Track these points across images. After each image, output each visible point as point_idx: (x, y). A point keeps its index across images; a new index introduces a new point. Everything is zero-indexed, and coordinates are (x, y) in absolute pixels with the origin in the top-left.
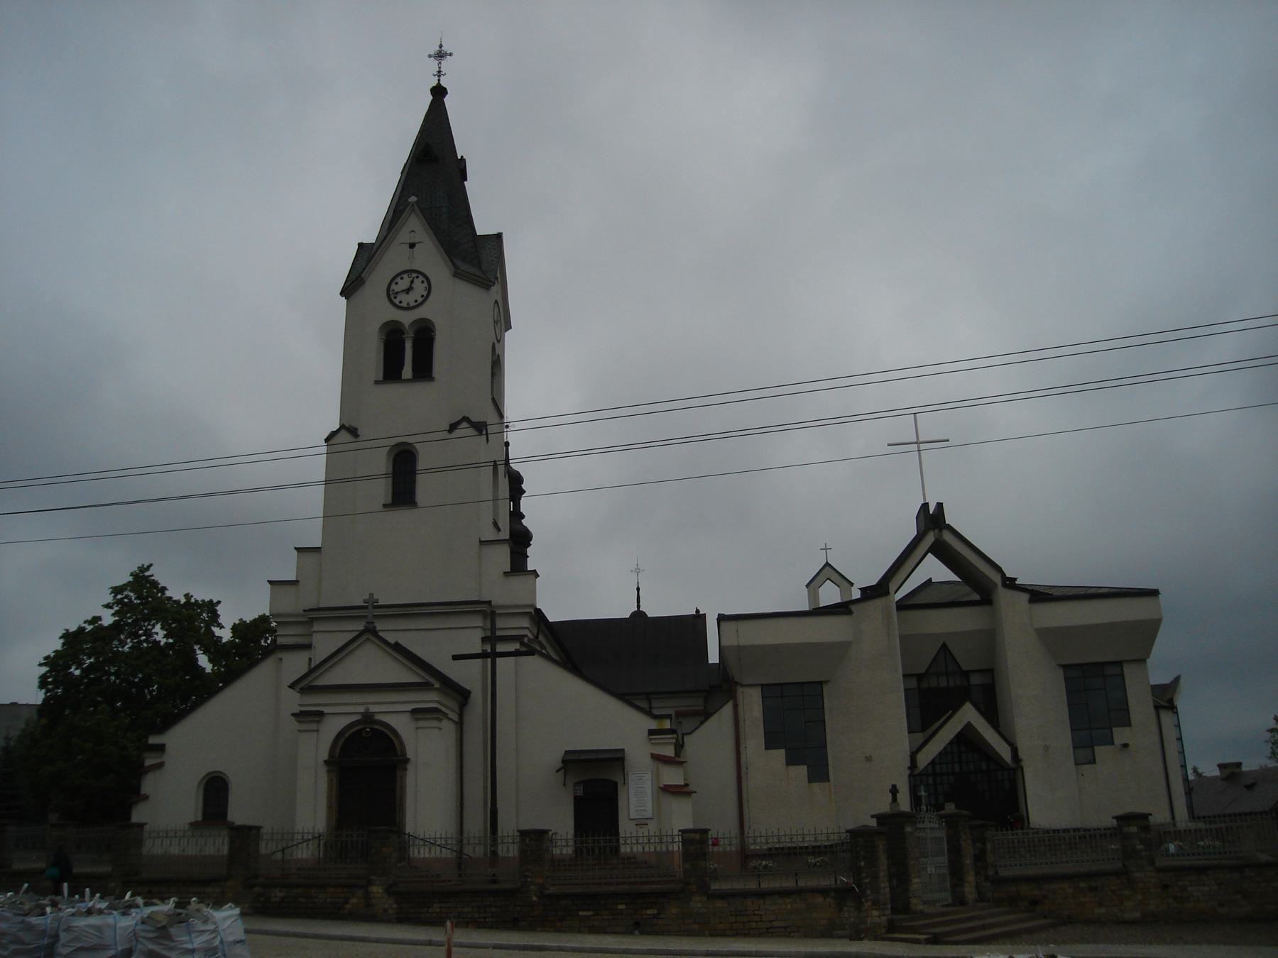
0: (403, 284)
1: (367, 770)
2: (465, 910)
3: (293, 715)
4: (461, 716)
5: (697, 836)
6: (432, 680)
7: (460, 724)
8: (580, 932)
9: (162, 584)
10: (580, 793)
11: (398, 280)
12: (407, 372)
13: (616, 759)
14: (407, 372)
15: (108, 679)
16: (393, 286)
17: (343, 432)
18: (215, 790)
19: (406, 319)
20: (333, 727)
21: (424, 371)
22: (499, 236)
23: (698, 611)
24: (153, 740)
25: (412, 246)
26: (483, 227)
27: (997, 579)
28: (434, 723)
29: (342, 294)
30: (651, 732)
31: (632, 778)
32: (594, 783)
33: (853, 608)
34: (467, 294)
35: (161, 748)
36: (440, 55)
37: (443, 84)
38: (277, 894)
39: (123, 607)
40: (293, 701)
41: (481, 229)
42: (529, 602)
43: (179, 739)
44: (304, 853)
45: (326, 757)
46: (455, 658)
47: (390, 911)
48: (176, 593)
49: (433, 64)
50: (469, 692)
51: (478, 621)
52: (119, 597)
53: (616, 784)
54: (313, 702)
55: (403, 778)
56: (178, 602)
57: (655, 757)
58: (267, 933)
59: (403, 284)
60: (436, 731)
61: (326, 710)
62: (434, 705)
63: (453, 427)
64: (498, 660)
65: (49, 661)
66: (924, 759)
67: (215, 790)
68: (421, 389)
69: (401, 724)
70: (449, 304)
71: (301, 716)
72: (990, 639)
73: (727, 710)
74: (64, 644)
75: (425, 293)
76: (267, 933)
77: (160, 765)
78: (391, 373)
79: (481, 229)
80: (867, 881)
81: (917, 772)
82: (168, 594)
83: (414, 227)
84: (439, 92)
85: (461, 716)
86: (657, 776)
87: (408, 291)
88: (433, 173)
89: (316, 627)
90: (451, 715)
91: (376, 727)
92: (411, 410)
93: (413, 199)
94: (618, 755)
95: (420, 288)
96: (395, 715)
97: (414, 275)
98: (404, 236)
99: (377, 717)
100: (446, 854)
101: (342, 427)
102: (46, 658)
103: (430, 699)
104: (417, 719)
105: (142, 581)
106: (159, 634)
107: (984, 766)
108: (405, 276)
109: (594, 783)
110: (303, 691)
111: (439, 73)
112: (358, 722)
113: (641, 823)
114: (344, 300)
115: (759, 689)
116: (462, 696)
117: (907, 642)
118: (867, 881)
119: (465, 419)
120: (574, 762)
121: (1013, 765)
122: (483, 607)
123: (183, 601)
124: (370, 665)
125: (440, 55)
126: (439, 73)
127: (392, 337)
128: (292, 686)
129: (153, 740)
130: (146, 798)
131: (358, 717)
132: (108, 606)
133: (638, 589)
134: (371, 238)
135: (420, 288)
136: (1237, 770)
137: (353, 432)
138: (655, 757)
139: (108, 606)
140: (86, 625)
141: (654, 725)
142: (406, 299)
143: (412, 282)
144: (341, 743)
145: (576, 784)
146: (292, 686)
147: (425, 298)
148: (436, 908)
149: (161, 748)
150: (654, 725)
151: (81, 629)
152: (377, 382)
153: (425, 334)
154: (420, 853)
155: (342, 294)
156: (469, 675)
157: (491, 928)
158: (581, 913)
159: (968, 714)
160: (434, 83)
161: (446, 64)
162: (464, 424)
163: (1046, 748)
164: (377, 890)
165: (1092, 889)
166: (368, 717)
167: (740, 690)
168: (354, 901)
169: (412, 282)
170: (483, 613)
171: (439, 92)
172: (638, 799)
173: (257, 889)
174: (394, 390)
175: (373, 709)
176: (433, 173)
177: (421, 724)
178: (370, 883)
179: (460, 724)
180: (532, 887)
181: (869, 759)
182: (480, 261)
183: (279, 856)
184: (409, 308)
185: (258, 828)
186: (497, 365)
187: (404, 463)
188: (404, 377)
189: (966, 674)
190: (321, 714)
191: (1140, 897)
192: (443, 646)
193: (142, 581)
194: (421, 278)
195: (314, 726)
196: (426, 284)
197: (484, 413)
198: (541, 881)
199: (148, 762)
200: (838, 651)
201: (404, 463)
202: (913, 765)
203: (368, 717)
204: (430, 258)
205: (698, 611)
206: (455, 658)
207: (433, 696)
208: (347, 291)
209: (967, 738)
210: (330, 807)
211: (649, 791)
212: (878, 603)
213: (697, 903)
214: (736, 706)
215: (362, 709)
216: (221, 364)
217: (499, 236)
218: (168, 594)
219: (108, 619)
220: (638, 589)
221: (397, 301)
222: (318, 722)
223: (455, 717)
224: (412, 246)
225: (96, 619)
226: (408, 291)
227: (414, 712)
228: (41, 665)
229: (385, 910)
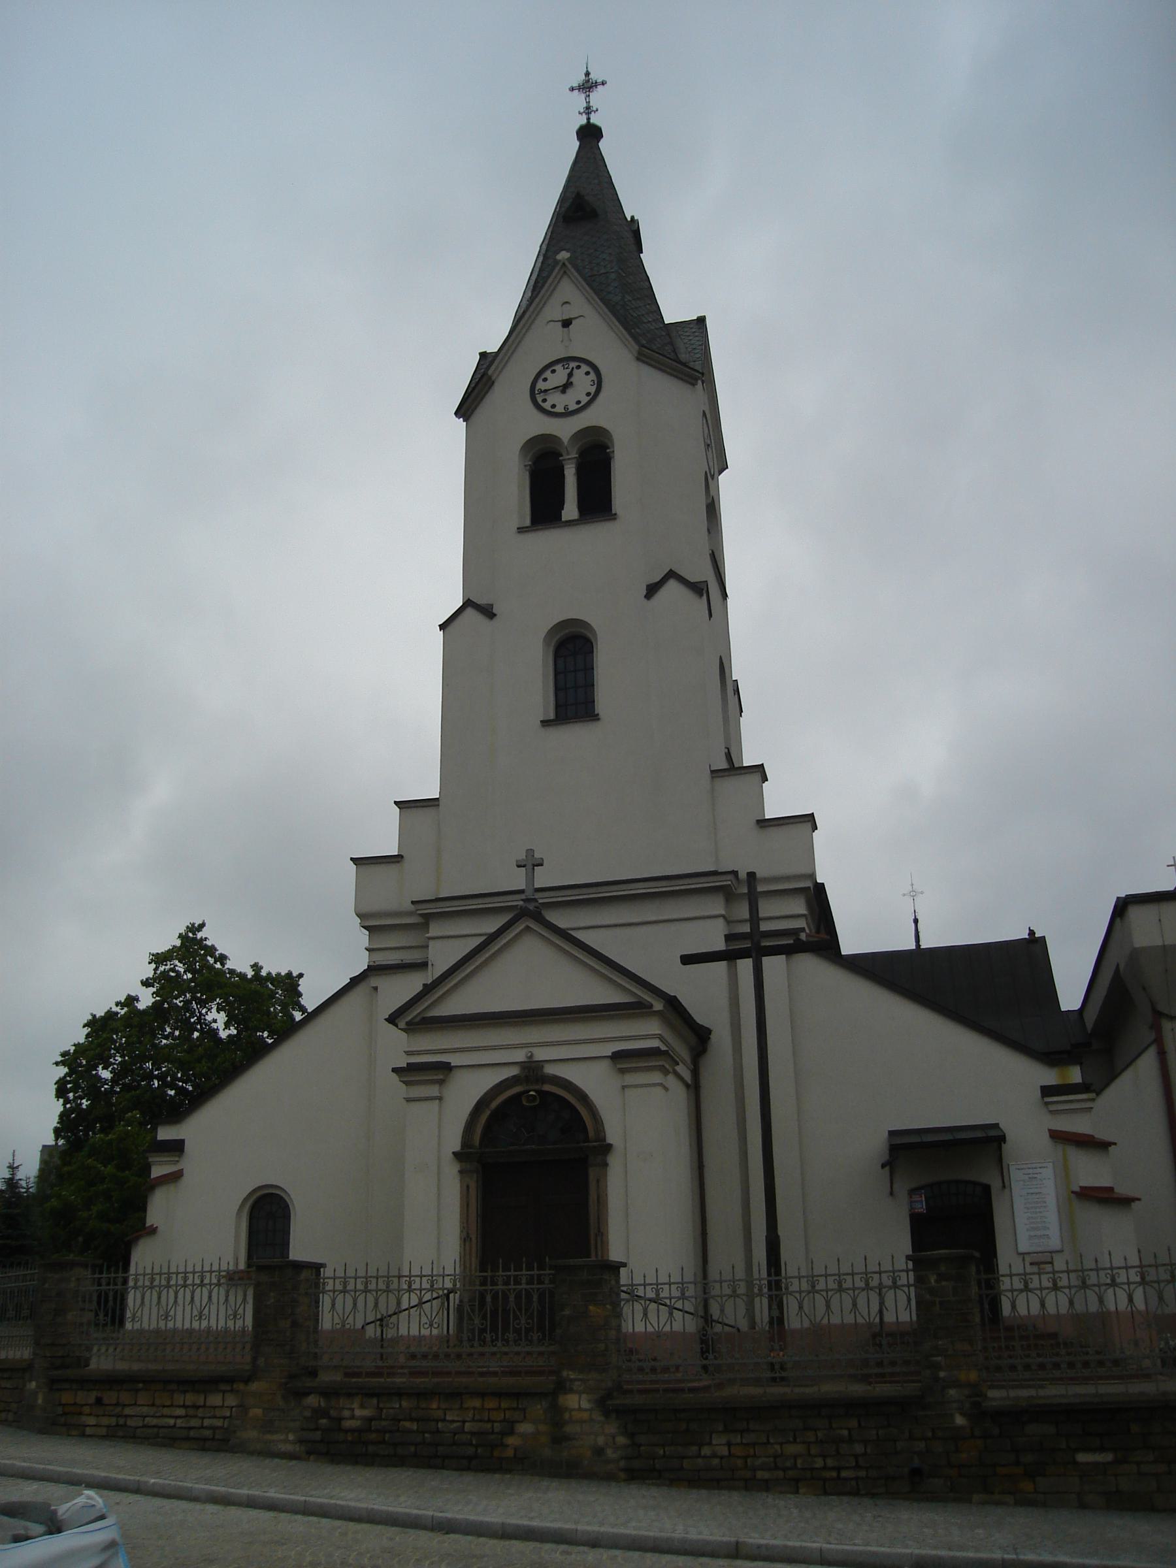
0: (559, 377)
1: (533, 1166)
2: (791, 1449)
3: (394, 1070)
4: (695, 1073)
6: (647, 997)
7: (694, 1088)
8: (1083, 1506)
9: (221, 950)
10: (921, 1207)
11: (548, 374)
12: (570, 510)
13: (988, 1142)
14: (570, 510)
15: (150, 1085)
16: (541, 385)
17: (470, 611)
18: (268, 1213)
19: (564, 430)
20: (467, 1091)
21: (597, 503)
22: (701, 321)
23: (1032, 933)
24: (165, 1133)
25: (567, 323)
26: (673, 310)
28: (656, 1077)
29: (458, 413)
30: (1047, 1091)
31: (1016, 1176)
32: (947, 1186)
34: (660, 388)
35: (177, 1147)
36: (588, 86)
38: (357, 1412)
39: (164, 983)
40: (397, 1046)
41: (670, 316)
42: (807, 871)
43: (200, 1130)
44: (419, 1325)
45: (457, 1147)
46: (687, 960)
47: (609, 1452)
48: (240, 963)
49: (579, 100)
50: (709, 1031)
51: (716, 906)
52: (162, 968)
53: (987, 1189)
54: (431, 1046)
55: (601, 1181)
56: (242, 976)
57: (1057, 1136)
58: (323, 1512)
59: (559, 377)
60: (659, 1090)
61: (454, 1060)
62: (655, 1043)
63: (652, 590)
64: (767, 961)
65: (67, 1059)
67: (268, 1213)
68: (596, 534)
69: (595, 1082)
70: (629, 405)
71: (409, 1072)
73: (1148, 1062)
74: (88, 1036)
75: (593, 390)
76: (323, 1512)
77: (176, 1177)
78: (544, 511)
79: (670, 316)
82: (229, 965)
83: (570, 295)
84: (590, 134)
85: (695, 1073)
86: (1065, 1172)
87: (565, 387)
88: (591, 235)
89: (435, 930)
90: (681, 1069)
91: (547, 1088)
92: (581, 570)
93: (564, 255)
94: (992, 1133)
95: (583, 383)
96: (582, 1064)
97: (573, 364)
98: (553, 311)
99: (550, 1070)
100: (248, 1367)
101: (467, 604)
102: (63, 1055)
103: (647, 1032)
104: (622, 1071)
105: (192, 946)
106: (217, 1018)
108: (558, 368)
109: (947, 1186)
110: (413, 1028)
111: (588, 110)
113: (1042, 1261)
114: (461, 424)
116: (700, 1037)
119: (672, 574)
120: (908, 1151)
122: (727, 881)
123: (250, 974)
124: (531, 975)
125: (588, 86)
126: (588, 110)
127: (543, 464)
128: (392, 1019)
129: (165, 1133)
130: (153, 1231)
132: (146, 983)
133: (916, 921)
134: (493, 347)
135: (583, 383)
137: (488, 612)
138: (1057, 1136)
139: (146, 983)
140: (118, 1009)
141: (1050, 1077)
142: (560, 401)
143: (570, 375)
144: (486, 1114)
145: (912, 1192)
146: (392, 1019)
147: (593, 397)
148: (719, 1444)
149: (177, 1147)
150: (1050, 1077)
151: (110, 1015)
152: (521, 530)
153: (596, 455)
154: (636, 1322)
155: (458, 413)
156: (706, 993)
157: (856, 1493)
158: (1082, 1457)
160: (583, 120)
161: (596, 97)
162: (672, 584)
164: (577, 1402)
166: (532, 1071)
168: (525, 1428)
169: (570, 375)
170: (728, 894)
171: (590, 134)
172: (1032, 1214)
173: (312, 1400)
174: (550, 539)
175: (540, 1054)
176: (591, 235)
177: (630, 1079)
178: (562, 1387)
179: (694, 1088)
182: (680, 354)
183: (371, 1331)
184: (568, 414)
185: (317, 1268)
186: (712, 510)
187: (572, 650)
190: (447, 1068)
192: (655, 948)
193: (192, 946)
194: (585, 368)
195: (433, 1090)
196: (593, 376)
197: (701, 572)
198: (973, 1376)
199: (157, 1172)
201: (572, 650)
203: (532, 1071)
204: (598, 338)
205: (1032, 933)
206: (687, 960)
207: (653, 1027)
208: (465, 410)
210: (465, 1239)
211: (1051, 1202)
214: (1162, 1054)
215: (520, 1056)
216: (300, 664)
217: (701, 321)
218: (229, 965)
219: (146, 999)
220: (916, 921)
221: (547, 406)
222: (441, 1082)
223: (687, 1076)
224: (567, 323)
225: (131, 1000)
226: (565, 387)
227: (617, 1057)
228: (57, 1064)
229: (599, 1451)
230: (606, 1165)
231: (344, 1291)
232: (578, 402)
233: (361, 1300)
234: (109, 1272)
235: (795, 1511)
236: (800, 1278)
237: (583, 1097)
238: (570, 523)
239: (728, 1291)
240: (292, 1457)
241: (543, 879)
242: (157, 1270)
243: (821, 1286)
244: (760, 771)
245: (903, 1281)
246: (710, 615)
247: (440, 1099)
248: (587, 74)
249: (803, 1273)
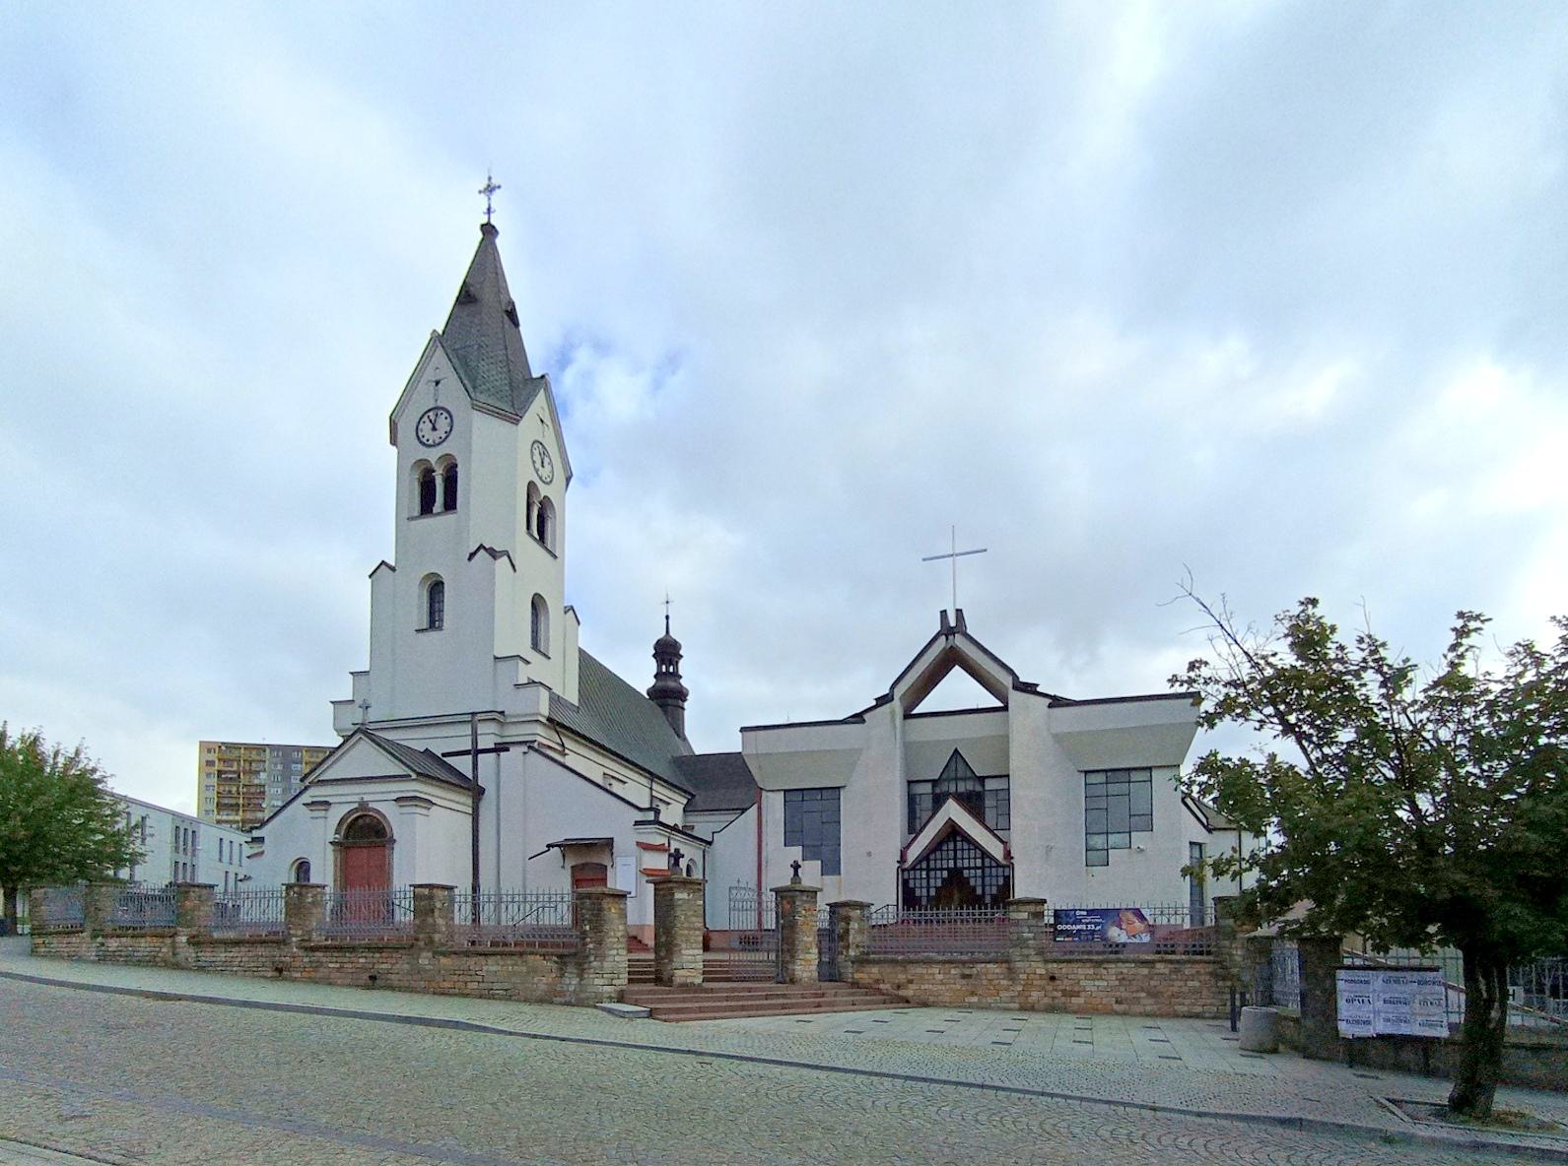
5: (426, 891)
6: (411, 773)
12: (438, 506)
19: (433, 456)
20: (337, 814)
27: (1008, 681)
30: (637, 823)
33: (866, 717)
36: (490, 189)
37: (493, 222)
47: (190, 959)
49: (483, 198)
61: (434, 800)
63: (472, 556)
66: (913, 854)
68: (451, 517)
69: (390, 812)
72: (1002, 745)
78: (426, 508)
80: (591, 946)
81: (906, 866)
84: (489, 230)
86: (639, 861)
88: (482, 312)
96: (382, 801)
99: (371, 805)
107: (979, 863)
112: (356, 810)
115: (783, 793)
117: (910, 750)
118: (591, 946)
121: (1004, 862)
131: (356, 805)
135: (443, 424)
136: (671, 684)
147: (448, 434)
159: (953, 811)
160: (485, 221)
161: (496, 195)
163: (1049, 849)
165: (965, 976)
166: (363, 805)
167: (764, 793)
171: (489, 230)
173: (100, 939)
174: (428, 521)
175: (366, 798)
180: (294, 939)
181: (869, 854)
188: (434, 511)
189: (982, 780)
190: (327, 803)
191: (1020, 988)
194: (445, 415)
195: (323, 813)
196: (420, 434)
200: (851, 758)
202: (903, 859)
203: (363, 805)
209: (953, 832)
212: (886, 708)
213: (425, 959)
215: (357, 798)
230: (393, 849)
231: (513, 902)
232: (422, 431)
233: (510, 907)
234: (980, 908)
235: (167, 978)
236: (507, 895)
237: (384, 817)
238: (438, 514)
239: (510, 900)
240: (93, 962)
241: (373, 715)
242: (540, 892)
243: (516, 899)
244: (681, 656)
245: (565, 899)
246: (515, 570)
247: (326, 818)
248: (490, 178)
249: (558, 892)
